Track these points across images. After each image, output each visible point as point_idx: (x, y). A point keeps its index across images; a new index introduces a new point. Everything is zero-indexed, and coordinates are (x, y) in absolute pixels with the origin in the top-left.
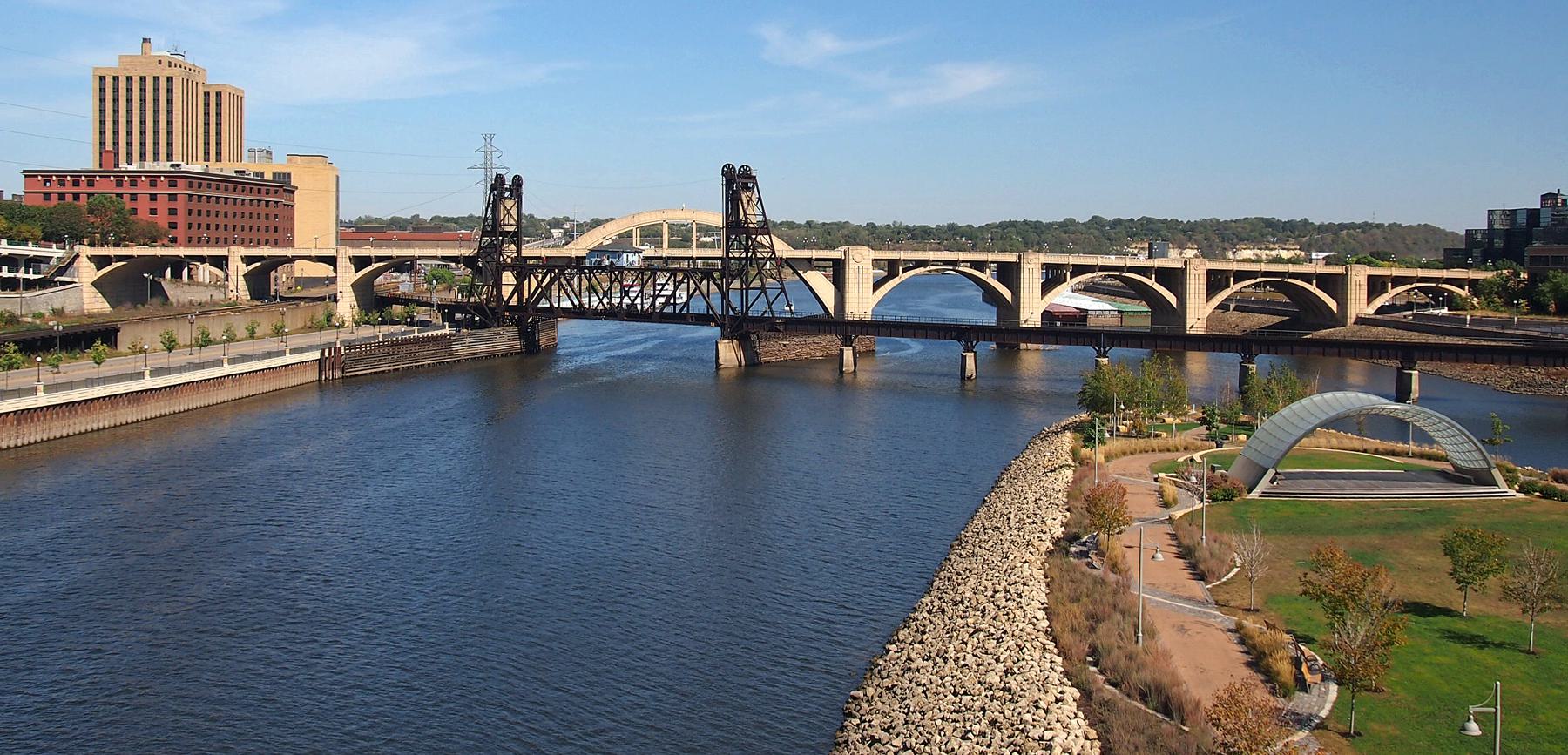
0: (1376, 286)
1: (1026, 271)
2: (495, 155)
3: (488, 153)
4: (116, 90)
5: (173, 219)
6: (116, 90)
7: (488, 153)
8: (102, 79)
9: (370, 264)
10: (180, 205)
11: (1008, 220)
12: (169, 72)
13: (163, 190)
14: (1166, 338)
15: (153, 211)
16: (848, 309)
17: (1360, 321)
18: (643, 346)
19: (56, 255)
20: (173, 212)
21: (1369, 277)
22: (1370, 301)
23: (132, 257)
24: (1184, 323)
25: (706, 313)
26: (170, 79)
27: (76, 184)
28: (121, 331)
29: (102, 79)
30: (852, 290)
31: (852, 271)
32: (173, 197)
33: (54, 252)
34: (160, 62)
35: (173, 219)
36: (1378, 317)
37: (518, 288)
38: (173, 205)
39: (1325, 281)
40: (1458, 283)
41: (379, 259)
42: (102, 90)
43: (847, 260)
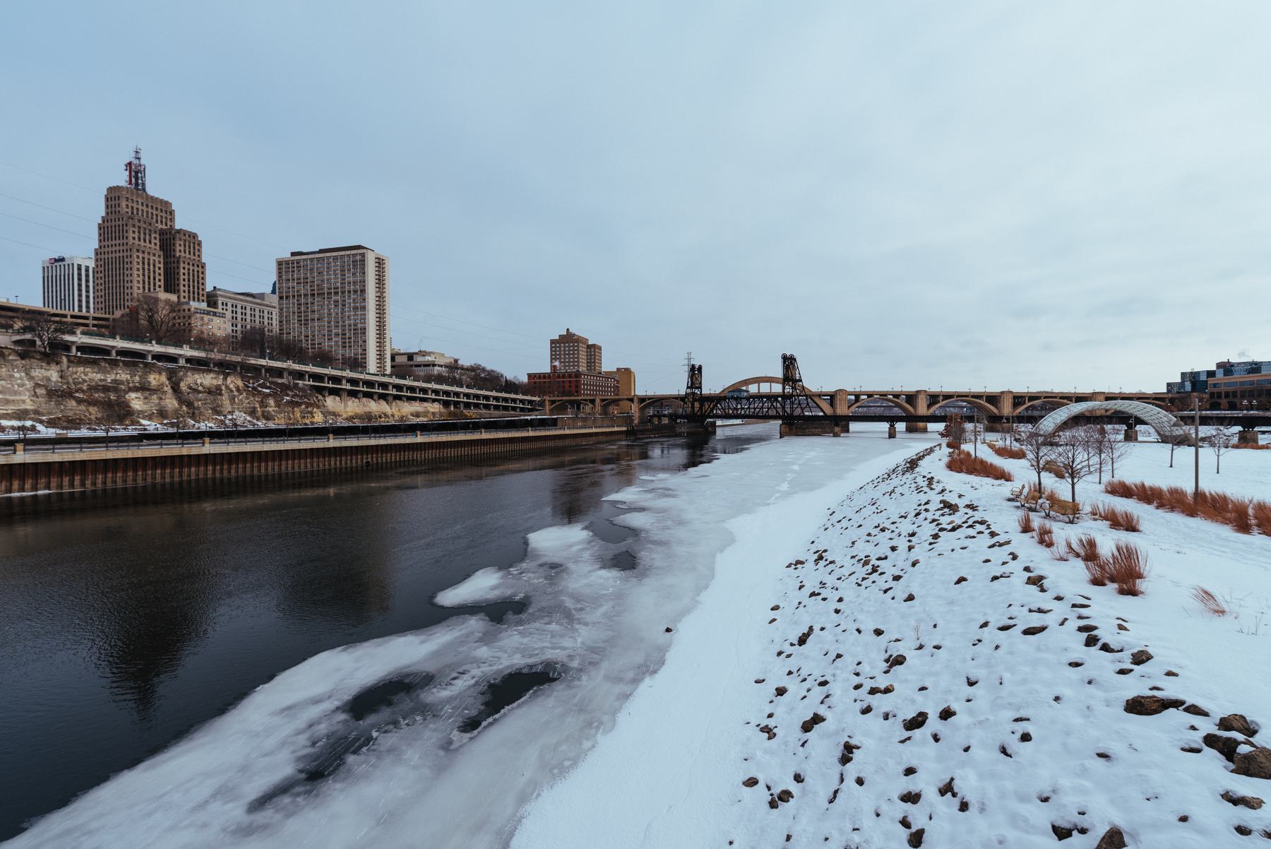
2: (692, 360)
3: (689, 359)
7: (689, 359)
22: (928, 410)
30: (838, 407)
37: (701, 408)
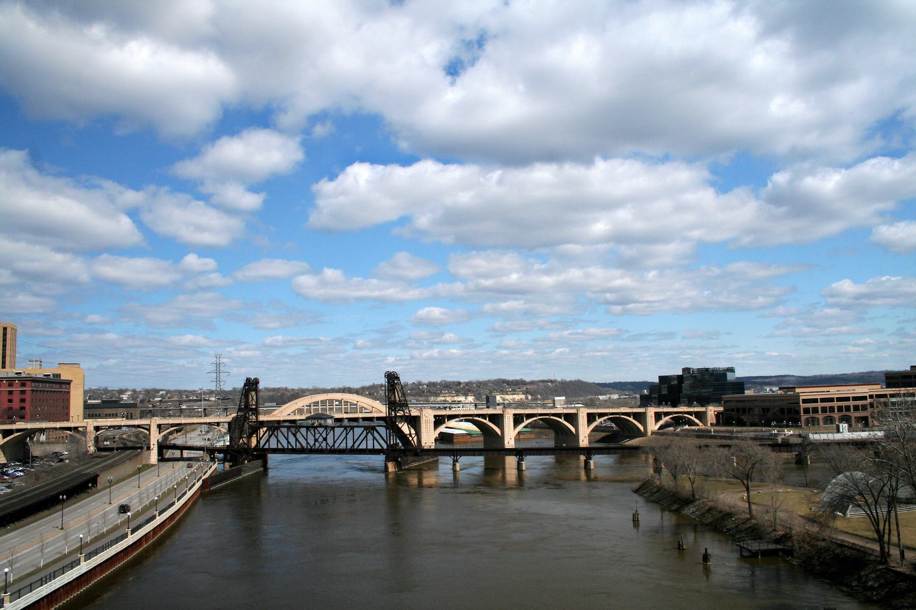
0: (658, 416)
1: (506, 418)
5: (23, 405)
9: (13, 434)
11: (380, 384)
13: (17, 388)
14: (567, 449)
17: (653, 433)
18: (5, 504)
20: (23, 400)
23: (27, 429)
24: (578, 442)
25: (372, 448)
28: (100, 476)
31: (424, 422)
32: (23, 392)
35: (23, 405)
36: (660, 431)
38: (23, 396)
39: (637, 416)
40: (690, 413)
41: (172, 425)
43: (422, 416)
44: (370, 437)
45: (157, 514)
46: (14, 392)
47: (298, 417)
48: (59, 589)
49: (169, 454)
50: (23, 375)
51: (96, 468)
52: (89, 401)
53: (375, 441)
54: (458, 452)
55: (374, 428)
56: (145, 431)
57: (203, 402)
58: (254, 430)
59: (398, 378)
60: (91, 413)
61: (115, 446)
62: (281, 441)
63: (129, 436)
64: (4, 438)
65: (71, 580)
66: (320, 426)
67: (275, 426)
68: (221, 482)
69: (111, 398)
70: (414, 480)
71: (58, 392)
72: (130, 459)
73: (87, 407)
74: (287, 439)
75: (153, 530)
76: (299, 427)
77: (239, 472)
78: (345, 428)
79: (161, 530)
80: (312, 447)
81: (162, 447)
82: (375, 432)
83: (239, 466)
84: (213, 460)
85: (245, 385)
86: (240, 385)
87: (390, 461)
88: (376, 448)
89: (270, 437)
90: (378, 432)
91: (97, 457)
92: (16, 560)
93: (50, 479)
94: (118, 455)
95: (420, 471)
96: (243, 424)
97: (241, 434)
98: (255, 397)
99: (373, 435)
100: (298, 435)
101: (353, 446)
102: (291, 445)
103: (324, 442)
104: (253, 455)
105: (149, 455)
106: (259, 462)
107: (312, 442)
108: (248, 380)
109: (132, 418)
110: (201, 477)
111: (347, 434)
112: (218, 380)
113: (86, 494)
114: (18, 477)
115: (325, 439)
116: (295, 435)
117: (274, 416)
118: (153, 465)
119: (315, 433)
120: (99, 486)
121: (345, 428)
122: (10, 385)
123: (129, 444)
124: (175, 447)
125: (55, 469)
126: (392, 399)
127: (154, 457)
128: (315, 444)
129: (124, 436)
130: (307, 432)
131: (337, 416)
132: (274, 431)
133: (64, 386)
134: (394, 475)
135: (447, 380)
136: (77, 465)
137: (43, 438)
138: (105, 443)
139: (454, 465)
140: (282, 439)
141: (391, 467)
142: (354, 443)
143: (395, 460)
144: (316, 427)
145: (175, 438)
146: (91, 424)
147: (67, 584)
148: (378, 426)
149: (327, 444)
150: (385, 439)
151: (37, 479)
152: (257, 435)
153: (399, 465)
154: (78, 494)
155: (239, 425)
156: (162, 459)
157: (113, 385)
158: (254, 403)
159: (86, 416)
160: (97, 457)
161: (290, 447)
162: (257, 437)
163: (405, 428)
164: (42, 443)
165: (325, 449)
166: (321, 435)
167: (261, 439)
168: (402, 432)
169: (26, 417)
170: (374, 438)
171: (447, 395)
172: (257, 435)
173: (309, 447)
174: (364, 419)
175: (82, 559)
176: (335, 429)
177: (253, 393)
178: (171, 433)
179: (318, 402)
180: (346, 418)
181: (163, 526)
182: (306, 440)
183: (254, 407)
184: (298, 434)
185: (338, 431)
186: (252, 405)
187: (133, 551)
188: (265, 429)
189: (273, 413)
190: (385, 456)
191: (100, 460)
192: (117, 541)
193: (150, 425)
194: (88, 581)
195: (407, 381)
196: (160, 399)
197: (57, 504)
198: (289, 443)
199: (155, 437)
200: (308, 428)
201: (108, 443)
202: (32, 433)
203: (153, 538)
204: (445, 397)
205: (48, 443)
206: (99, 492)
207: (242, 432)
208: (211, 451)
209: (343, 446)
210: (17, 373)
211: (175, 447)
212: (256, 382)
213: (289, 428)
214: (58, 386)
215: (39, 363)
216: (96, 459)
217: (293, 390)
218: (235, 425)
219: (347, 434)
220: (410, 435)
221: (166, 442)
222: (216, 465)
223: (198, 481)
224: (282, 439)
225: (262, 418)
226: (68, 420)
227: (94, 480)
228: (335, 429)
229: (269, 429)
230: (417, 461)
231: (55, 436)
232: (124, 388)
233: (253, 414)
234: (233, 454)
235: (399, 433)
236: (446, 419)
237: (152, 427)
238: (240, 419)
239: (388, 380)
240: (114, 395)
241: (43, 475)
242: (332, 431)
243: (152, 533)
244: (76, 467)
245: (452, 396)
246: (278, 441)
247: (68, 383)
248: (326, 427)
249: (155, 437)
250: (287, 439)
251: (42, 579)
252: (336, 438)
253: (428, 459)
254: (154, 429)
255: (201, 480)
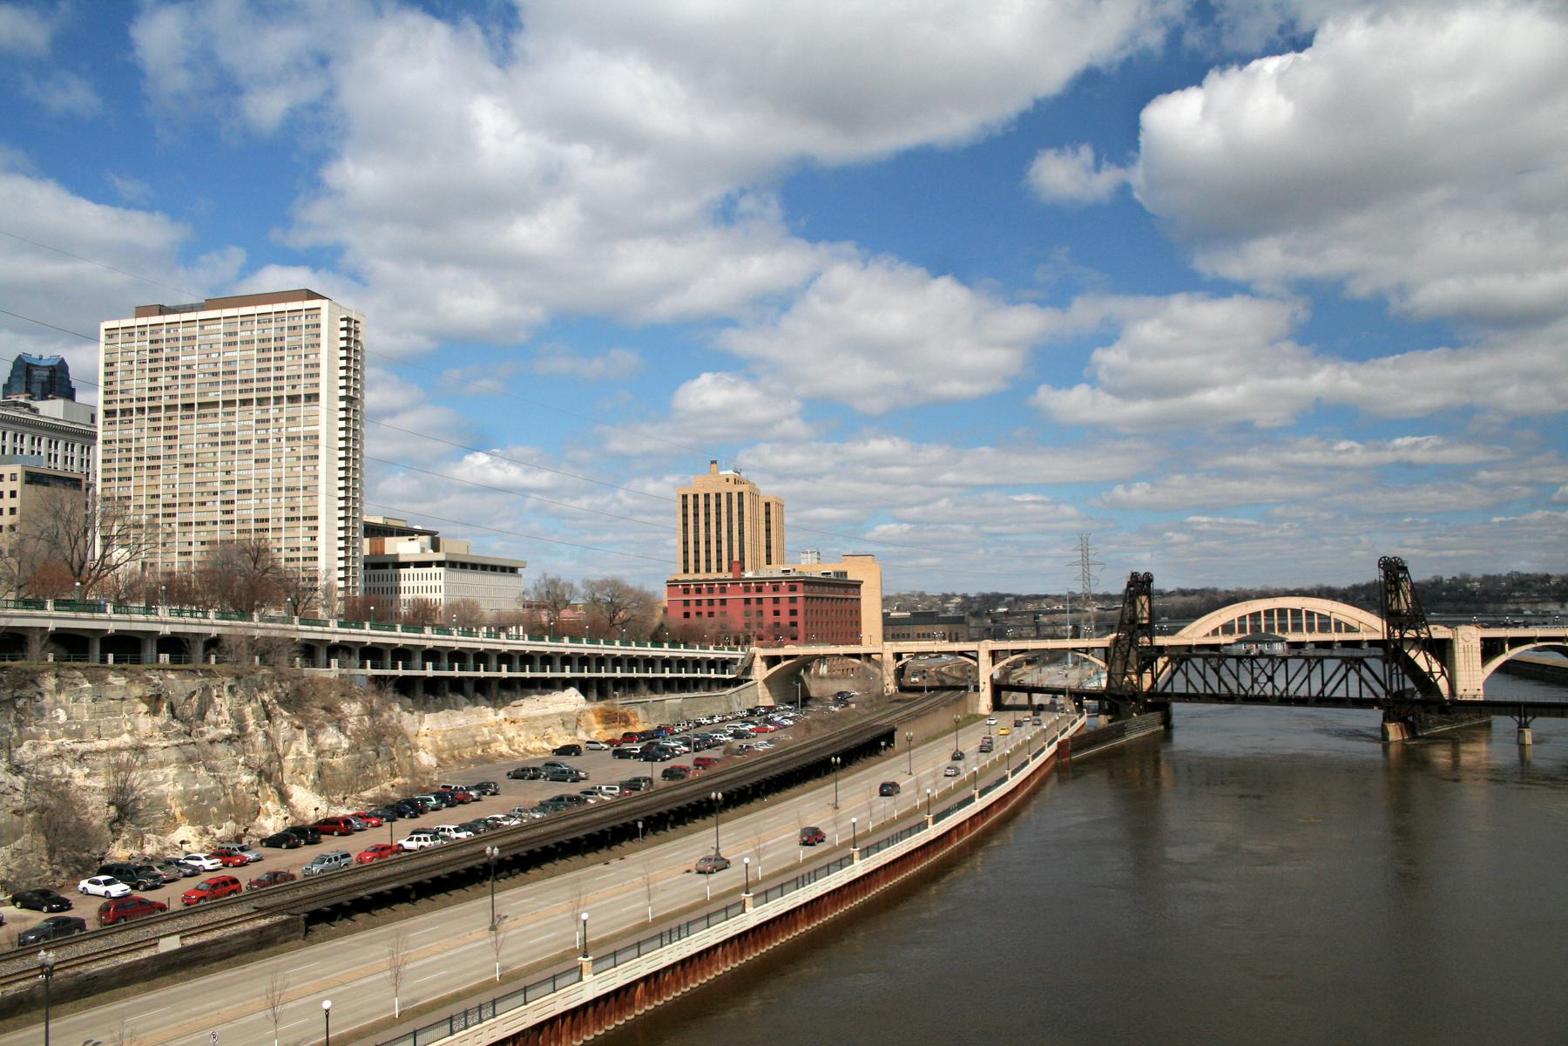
4: (696, 506)
5: (794, 619)
6: (696, 506)
8: (685, 497)
10: (800, 606)
12: (740, 488)
13: (784, 594)
15: (777, 613)
16: (1460, 692)
19: (741, 657)
20: (793, 612)
21: (1482, 639)
26: (740, 495)
27: (699, 591)
29: (685, 497)
31: (1461, 650)
33: (739, 654)
34: (727, 480)
35: (794, 619)
38: (794, 606)
42: (685, 507)
44: (1353, 676)
45: (977, 795)
46: (764, 601)
47: (1222, 639)
48: (822, 897)
49: (1010, 698)
50: (792, 574)
51: (893, 717)
52: (892, 614)
53: (1363, 684)
54: (1529, 709)
55: (1360, 661)
56: (971, 661)
57: (1068, 614)
58: (1148, 659)
59: (1404, 569)
60: (921, 632)
61: (925, 684)
62: (1210, 682)
63: (951, 669)
64: (769, 667)
65: (840, 885)
66: (1262, 655)
67: (1182, 656)
68: (1089, 746)
69: (930, 608)
70: (1441, 756)
71: (842, 599)
72: (946, 706)
73: (887, 621)
74: (1203, 677)
75: (970, 819)
76: (1223, 658)
77: (1121, 731)
78: (1307, 659)
79: (983, 820)
80: (1247, 692)
81: (998, 689)
82: (1362, 667)
83: (1120, 722)
84: (1080, 709)
85: (1130, 585)
86: (1119, 587)
87: (1391, 721)
88: (1364, 696)
89: (1174, 673)
90: (1367, 667)
91: (898, 701)
92: (765, 851)
93: (826, 732)
94: (928, 698)
95: (1454, 741)
96: (1129, 651)
97: (1125, 668)
98: (1146, 606)
99: (1358, 672)
100: (1223, 671)
101: (1322, 691)
102: (1210, 688)
103: (1270, 684)
104: (1146, 704)
105: (978, 699)
106: (1155, 717)
107: (1246, 682)
108: (1134, 576)
109: (957, 640)
110: (1056, 738)
111: (1310, 671)
112: (1086, 578)
113: (877, 758)
114: (786, 726)
115: (1271, 679)
116: (1217, 671)
117: (1182, 637)
118: (985, 717)
119: (1252, 668)
120: (897, 745)
121: (1307, 659)
122: (776, 589)
123: (949, 682)
124: (1020, 688)
125: (834, 718)
126: (1395, 607)
127: (985, 700)
128: (1252, 687)
129: (943, 669)
130: (1238, 666)
131: (1292, 637)
132: (1181, 664)
133: (851, 590)
134: (1400, 747)
135: (1229, 589)
136: (867, 712)
137: (823, 670)
138: (913, 679)
139: (1521, 733)
140: (1195, 678)
141: (1394, 732)
142: (1324, 685)
143: (1400, 719)
144: (1254, 658)
145: (1025, 674)
146: (891, 648)
147: (834, 891)
148: (1368, 657)
149: (1274, 686)
150: (1382, 678)
151: (809, 730)
152: (1152, 669)
153: (1411, 729)
154: (864, 757)
155: (1122, 653)
156: (998, 706)
157: (934, 589)
158: (1145, 615)
159: (890, 636)
160: (898, 701)
161: (1209, 691)
162: (1152, 673)
163: (1421, 660)
164: (822, 678)
165: (1271, 697)
166: (1263, 671)
167: (1158, 676)
168: (1417, 668)
169: (799, 638)
170: (1361, 679)
171: (1523, 600)
172: (1152, 669)
173: (1242, 693)
174: (1345, 644)
175: (856, 856)
176: (1289, 661)
177: (1144, 598)
178: (1016, 665)
179: (1258, 613)
180: (1311, 642)
181: (987, 815)
182: (1237, 679)
183: (1145, 622)
184: (1223, 668)
185: (1294, 665)
186: (1142, 618)
187: (937, 849)
188: (1166, 659)
189: (1181, 633)
190: (1382, 711)
191: (901, 705)
192: (910, 831)
193: (977, 652)
194: (866, 890)
195: (1440, 574)
196: (1005, 610)
197: (826, 773)
198: (1206, 683)
199: (987, 672)
200: (1239, 658)
201: (917, 679)
202: (806, 662)
203: (971, 831)
204: (1517, 603)
205: (831, 678)
206: (896, 755)
207: (1126, 664)
208: (1078, 696)
209: (1303, 692)
210: (784, 571)
211: (1020, 688)
212: (1148, 579)
213: (1206, 658)
214: (842, 590)
215: (815, 555)
216: (896, 704)
217: (1227, 592)
218: (1115, 652)
219: (1310, 671)
220: (1431, 672)
221: (1007, 678)
222: (1085, 718)
223: (1049, 744)
224: (1195, 678)
225: (1160, 641)
226: (859, 643)
227: (889, 736)
228: (1326, 661)
229: (1172, 659)
230: (1446, 723)
231: (841, 668)
232: (949, 592)
233: (1145, 634)
234: (1114, 701)
235: (1411, 667)
236: (1507, 646)
237: (980, 655)
238: (1123, 642)
239: (1386, 573)
240: (935, 603)
241: (817, 725)
242: (1319, 665)
243: (967, 824)
244: (865, 716)
245: (1532, 603)
246: (1188, 681)
247: (857, 585)
248: (1272, 658)
249: (987, 672)
250: (1203, 677)
251: (797, 879)
252: (1326, 679)
253: (1470, 719)
254: (984, 657)
255: (1055, 744)
